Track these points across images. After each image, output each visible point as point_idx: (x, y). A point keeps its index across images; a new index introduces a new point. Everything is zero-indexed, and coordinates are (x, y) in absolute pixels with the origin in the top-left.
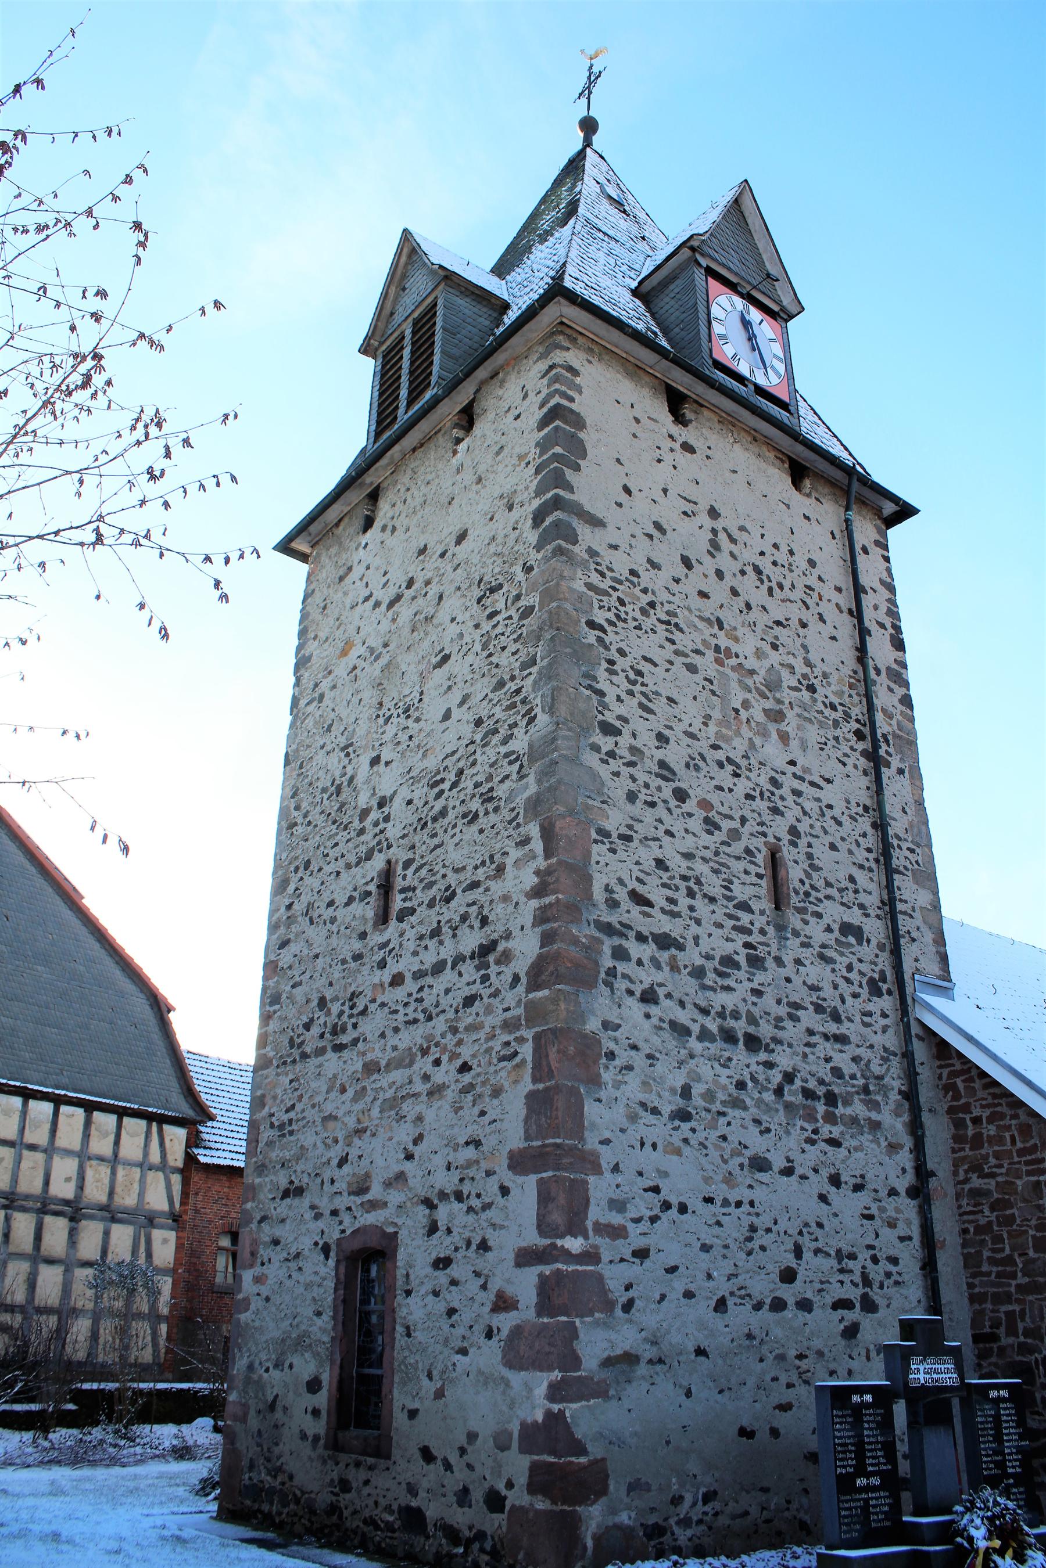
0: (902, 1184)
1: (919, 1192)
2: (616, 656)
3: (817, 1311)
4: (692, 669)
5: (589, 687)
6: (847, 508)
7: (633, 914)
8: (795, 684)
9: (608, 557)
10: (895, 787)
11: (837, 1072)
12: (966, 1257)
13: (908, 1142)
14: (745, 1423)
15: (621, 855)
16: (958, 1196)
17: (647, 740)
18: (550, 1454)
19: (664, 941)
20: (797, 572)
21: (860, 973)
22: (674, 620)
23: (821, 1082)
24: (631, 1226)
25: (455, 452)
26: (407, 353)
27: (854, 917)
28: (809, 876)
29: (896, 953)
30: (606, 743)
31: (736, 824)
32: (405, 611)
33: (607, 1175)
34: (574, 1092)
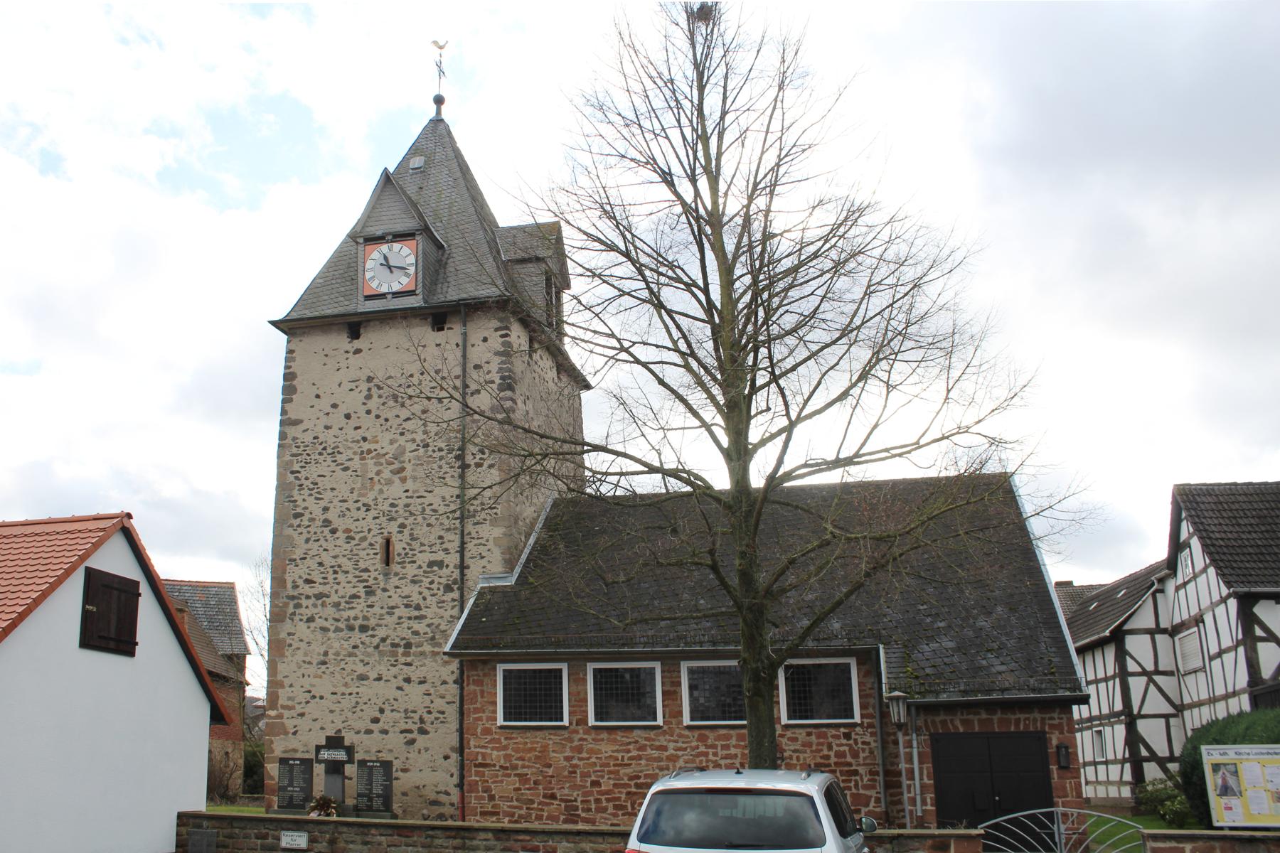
3: (390, 734)
7: (307, 590)
15: (301, 566)
19: (319, 596)
24: (297, 706)
30: (296, 522)
33: (287, 688)
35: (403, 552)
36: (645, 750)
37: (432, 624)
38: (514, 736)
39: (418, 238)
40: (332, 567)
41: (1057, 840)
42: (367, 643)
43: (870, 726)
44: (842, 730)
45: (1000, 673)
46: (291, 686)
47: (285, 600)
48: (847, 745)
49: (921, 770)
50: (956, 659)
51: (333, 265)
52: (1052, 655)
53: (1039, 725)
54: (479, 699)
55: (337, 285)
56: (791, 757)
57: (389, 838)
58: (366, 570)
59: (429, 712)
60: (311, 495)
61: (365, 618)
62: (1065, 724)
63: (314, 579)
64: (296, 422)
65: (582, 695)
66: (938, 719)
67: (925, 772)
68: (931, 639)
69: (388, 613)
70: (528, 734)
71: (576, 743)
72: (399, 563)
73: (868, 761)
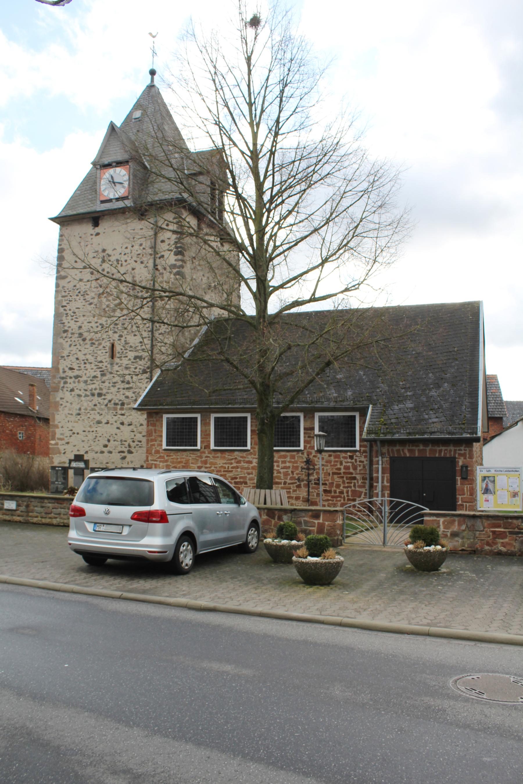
3: (113, 454)
7: (70, 373)
15: (67, 360)
19: (77, 377)
30: (65, 335)
35: (121, 351)
36: (240, 463)
37: (136, 392)
38: (171, 454)
39: (130, 164)
40: (83, 360)
41: (383, 515)
42: (102, 403)
43: (365, 452)
44: (349, 454)
45: (433, 423)
46: (62, 427)
47: (59, 379)
48: (351, 462)
49: (383, 478)
50: (410, 414)
51: (86, 182)
52: (467, 413)
53: (452, 453)
54: (154, 434)
55: (88, 195)
56: (319, 469)
57: (53, 505)
58: (101, 362)
59: (134, 442)
60: (72, 319)
61: (101, 389)
62: (467, 453)
63: (74, 368)
64: (64, 278)
65: (208, 433)
66: (395, 449)
67: (385, 479)
68: (400, 402)
69: (113, 386)
70: (179, 454)
71: (204, 459)
72: (119, 358)
73: (362, 472)
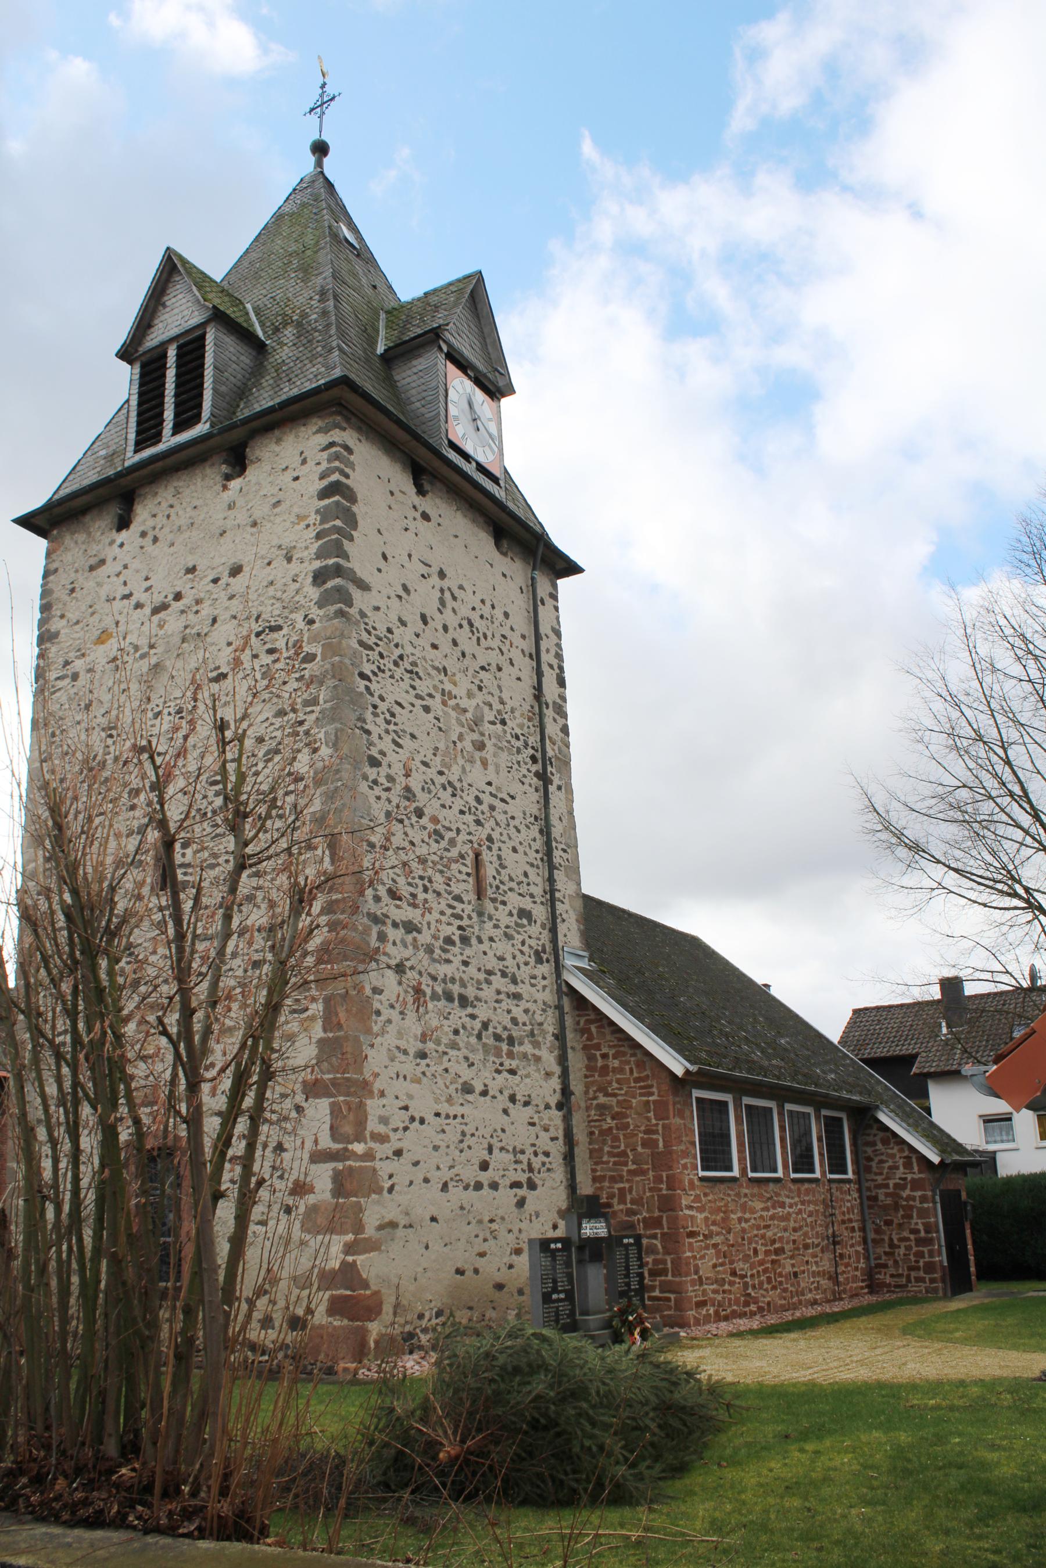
0: (553, 1101)
1: (565, 1104)
2: (378, 702)
4: (427, 709)
5: (362, 728)
6: (534, 569)
8: (492, 719)
9: (373, 617)
10: (556, 798)
11: (514, 1021)
12: (591, 1151)
13: (557, 1070)
14: (459, 1265)
16: (588, 1109)
17: (397, 770)
18: (346, 1289)
19: (410, 927)
20: (497, 623)
21: (530, 947)
22: (415, 669)
23: (505, 1028)
24: (391, 1134)
25: (225, 488)
26: (171, 374)
27: (526, 904)
28: (499, 873)
29: (554, 930)
30: (372, 773)
31: (453, 834)
32: (174, 622)
34: (357, 1040)
